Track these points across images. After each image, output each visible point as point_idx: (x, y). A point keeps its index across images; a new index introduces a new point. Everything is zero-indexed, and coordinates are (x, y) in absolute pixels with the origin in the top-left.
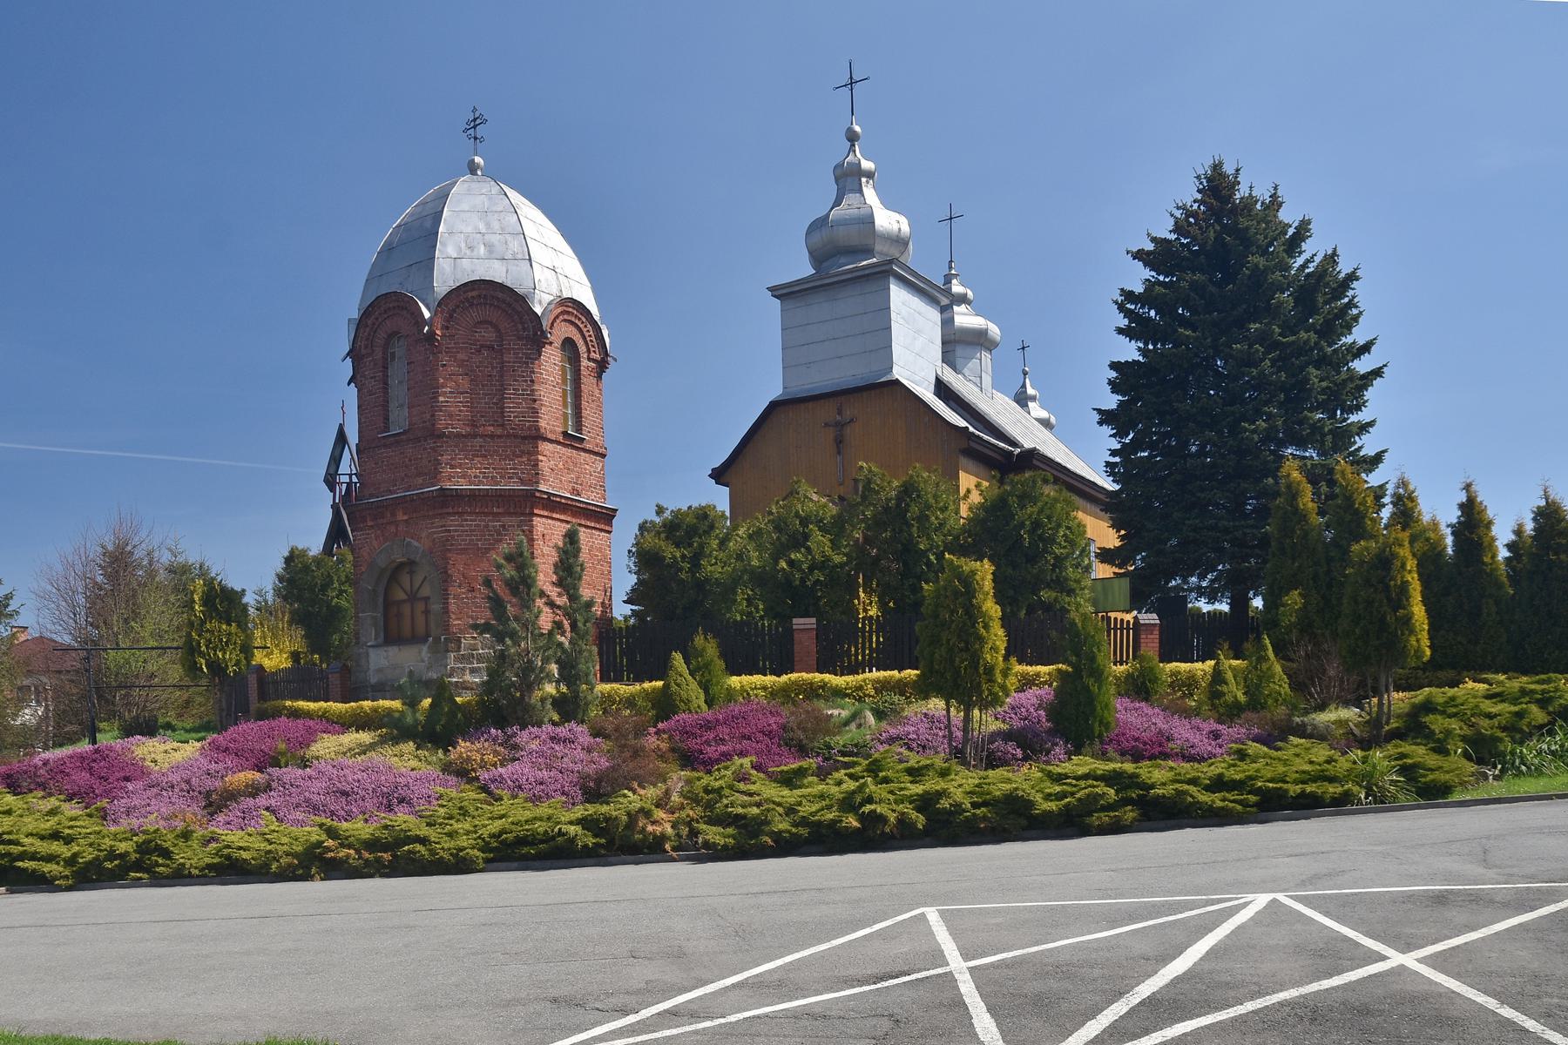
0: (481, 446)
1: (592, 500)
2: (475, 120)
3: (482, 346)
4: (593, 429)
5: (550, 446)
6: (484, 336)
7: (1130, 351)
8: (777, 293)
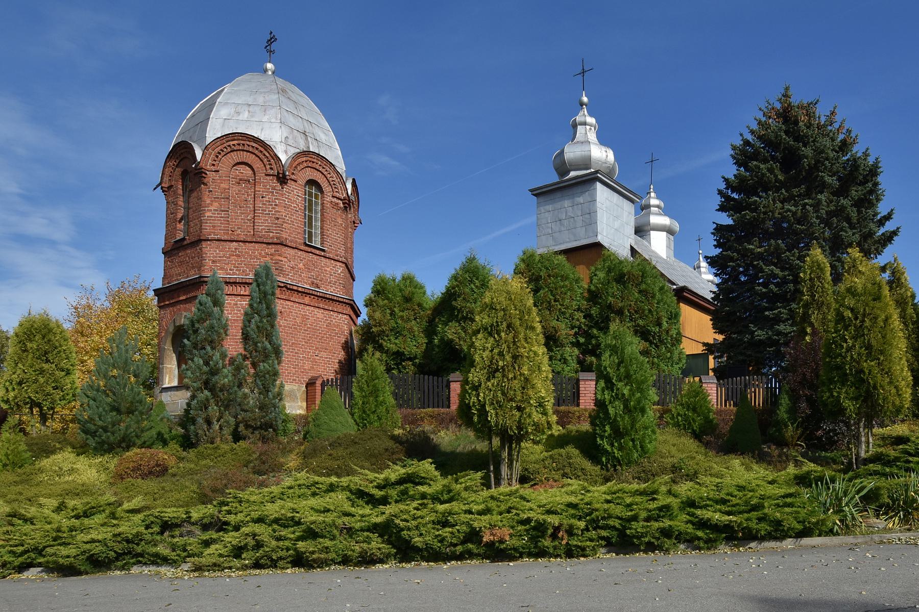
0: (236, 249)
1: (331, 292)
2: (271, 38)
3: (241, 180)
4: (333, 244)
5: (292, 251)
6: (242, 173)
7: (725, 220)
8: (534, 193)
